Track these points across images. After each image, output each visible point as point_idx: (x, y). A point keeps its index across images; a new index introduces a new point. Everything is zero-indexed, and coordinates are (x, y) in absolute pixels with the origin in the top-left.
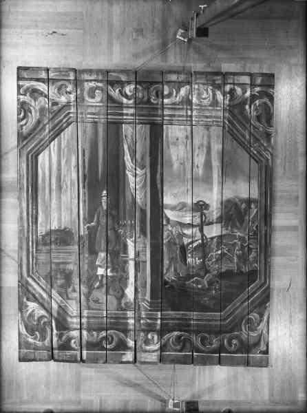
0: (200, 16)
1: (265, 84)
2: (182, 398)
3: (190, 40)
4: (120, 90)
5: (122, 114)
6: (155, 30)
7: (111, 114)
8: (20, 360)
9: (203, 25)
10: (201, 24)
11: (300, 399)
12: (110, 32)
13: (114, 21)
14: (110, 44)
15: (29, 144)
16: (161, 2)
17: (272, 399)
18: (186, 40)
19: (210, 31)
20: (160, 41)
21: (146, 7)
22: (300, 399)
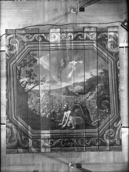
0: (81, 3)
1: (28, 33)
2: (75, 162)
3: (77, 13)
4: (36, 36)
5: (66, 46)
6: (62, 9)
7: (37, 47)
8: (7, 153)
9: (83, 6)
10: (82, 6)
11: (126, 162)
12: (44, 10)
13: (45, 6)
14: (44, 16)
15: (13, 61)
16: (47, 1)
17: (114, 162)
18: (75, 13)
19: (85, 8)
20: (65, 13)
21: (4, 13)
22: (126, 162)
